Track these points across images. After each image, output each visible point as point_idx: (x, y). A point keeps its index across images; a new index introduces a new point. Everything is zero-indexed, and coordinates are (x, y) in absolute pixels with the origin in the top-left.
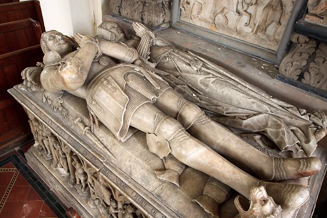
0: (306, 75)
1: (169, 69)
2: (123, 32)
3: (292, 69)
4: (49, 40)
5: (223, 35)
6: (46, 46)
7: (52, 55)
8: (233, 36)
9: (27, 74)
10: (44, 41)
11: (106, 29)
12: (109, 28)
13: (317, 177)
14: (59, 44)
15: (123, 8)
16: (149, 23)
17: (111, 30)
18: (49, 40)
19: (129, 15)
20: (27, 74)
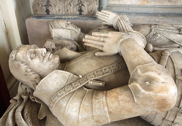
0: (50, 9)
1: (164, 45)
2: (78, 27)
3: (72, 8)
4: (32, 59)
5: (155, 6)
6: (29, 70)
7: (57, 78)
8: (165, 4)
9: (19, 114)
10: (22, 63)
11: (62, 28)
12: (64, 26)
13: (142, 106)
14: (49, 59)
15: (53, 5)
16: (89, 13)
17: (68, 28)
18: (32, 59)
19: (61, 11)
20: (19, 114)
